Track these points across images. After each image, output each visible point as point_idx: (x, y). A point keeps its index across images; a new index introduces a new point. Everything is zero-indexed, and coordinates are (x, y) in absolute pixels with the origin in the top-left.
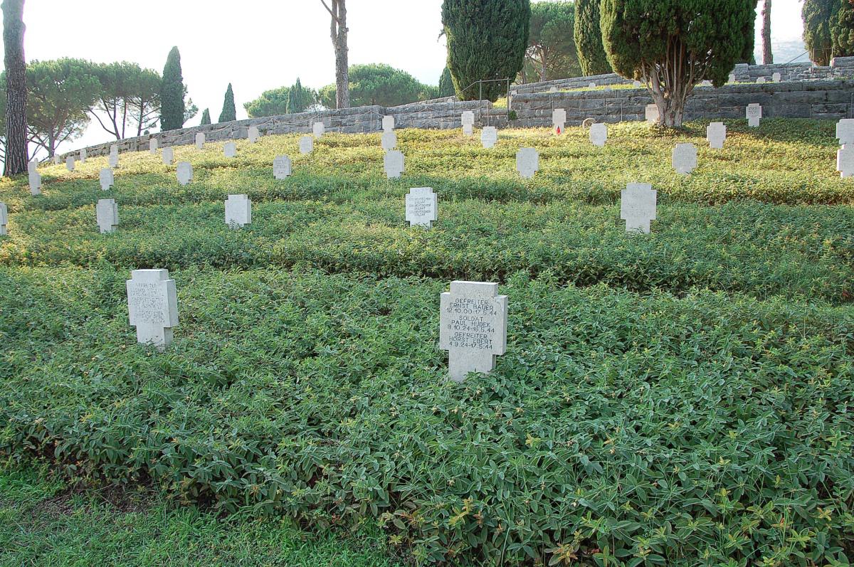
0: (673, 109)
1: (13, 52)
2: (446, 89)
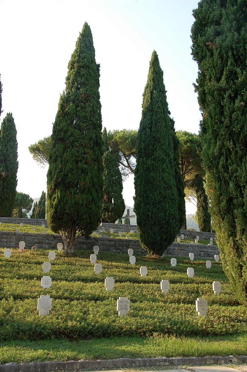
0: (71, 246)
1: (207, 279)
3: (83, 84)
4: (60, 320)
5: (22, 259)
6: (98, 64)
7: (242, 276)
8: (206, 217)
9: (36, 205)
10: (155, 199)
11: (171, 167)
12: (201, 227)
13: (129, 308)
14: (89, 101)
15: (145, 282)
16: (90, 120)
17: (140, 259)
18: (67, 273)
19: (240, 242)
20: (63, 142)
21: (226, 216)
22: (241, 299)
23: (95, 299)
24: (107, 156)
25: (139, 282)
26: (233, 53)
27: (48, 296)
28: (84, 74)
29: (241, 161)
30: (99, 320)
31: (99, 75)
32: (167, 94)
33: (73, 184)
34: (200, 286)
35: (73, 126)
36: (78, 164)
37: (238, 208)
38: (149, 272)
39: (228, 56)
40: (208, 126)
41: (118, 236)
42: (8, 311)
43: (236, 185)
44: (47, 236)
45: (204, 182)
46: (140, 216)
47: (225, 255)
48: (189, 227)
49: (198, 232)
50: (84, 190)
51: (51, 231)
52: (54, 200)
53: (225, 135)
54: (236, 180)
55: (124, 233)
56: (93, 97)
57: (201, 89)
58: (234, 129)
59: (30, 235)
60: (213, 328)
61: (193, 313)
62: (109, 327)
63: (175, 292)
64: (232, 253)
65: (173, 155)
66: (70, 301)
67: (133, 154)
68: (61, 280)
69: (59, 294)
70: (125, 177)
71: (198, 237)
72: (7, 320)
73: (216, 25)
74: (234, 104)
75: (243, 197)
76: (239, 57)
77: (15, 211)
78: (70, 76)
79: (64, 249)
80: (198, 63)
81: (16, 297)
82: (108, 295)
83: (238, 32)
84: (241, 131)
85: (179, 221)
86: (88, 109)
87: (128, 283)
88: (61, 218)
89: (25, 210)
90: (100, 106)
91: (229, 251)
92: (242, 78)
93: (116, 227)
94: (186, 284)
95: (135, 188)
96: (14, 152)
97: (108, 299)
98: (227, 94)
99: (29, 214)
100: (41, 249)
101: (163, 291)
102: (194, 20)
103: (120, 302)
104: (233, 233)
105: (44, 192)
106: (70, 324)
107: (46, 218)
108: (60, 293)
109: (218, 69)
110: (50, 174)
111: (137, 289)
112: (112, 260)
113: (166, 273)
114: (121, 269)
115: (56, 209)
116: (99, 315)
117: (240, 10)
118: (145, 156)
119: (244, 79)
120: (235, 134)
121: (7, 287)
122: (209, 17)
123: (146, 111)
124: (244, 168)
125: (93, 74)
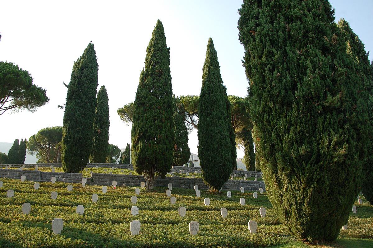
2: (12, 155)
3: (158, 63)
4: (147, 239)
5: (115, 194)
6: (169, 47)
7: (283, 203)
8: (252, 160)
9: (122, 154)
10: (214, 147)
11: (225, 123)
12: (248, 168)
13: (198, 229)
14: (162, 75)
15: (208, 210)
16: (164, 89)
17: (203, 193)
18: (149, 204)
19: (281, 177)
20: (143, 106)
21: (270, 158)
22: (281, 219)
23: (172, 223)
24: (176, 116)
25: (204, 210)
26: (269, 39)
27: (137, 221)
28: (159, 55)
29: (280, 117)
30: (177, 238)
31: (169, 56)
32: (220, 68)
33: (152, 137)
34: (250, 211)
35: (151, 93)
36: (155, 122)
37: (279, 152)
38: (211, 203)
39: (266, 41)
40: (254, 91)
41: (186, 176)
42: (109, 231)
43: (276, 134)
44: (133, 176)
45: (252, 133)
46: (202, 160)
47: (269, 187)
48: (238, 168)
49: (246, 172)
50: (160, 142)
51: (135, 172)
52: (138, 150)
53: (267, 98)
54: (277, 131)
55: (190, 173)
56: (165, 72)
57: (247, 64)
58: (273, 93)
59: (120, 176)
60: (262, 241)
61: (246, 231)
62: (184, 243)
63: (232, 217)
64: (275, 185)
65: (227, 114)
66: (153, 225)
67: (196, 113)
68: (145, 209)
69: (144, 220)
70: (189, 131)
71: (246, 175)
72: (109, 238)
73: (256, 19)
74: (273, 75)
75: (282, 144)
76: (274, 42)
77: (108, 158)
78: (148, 57)
79: (145, 186)
80: (244, 45)
81: (114, 222)
82: (181, 220)
83: (272, 24)
84: (279, 94)
85: (232, 163)
86: (162, 81)
87: (196, 211)
88: (143, 163)
89: (115, 157)
90: (171, 78)
91: (273, 184)
92: (278, 56)
93: (184, 169)
94: (239, 211)
95: (199, 139)
96: (106, 114)
97: (182, 222)
98: (267, 68)
99: (118, 161)
100: (129, 187)
101: (222, 216)
102: (239, 16)
103: (192, 225)
104: (275, 170)
105: (129, 144)
106: (155, 241)
107: (130, 164)
108: (146, 219)
109: (259, 50)
110: (134, 131)
111: (203, 215)
112: (182, 194)
113: (224, 203)
114: (190, 201)
115: (139, 156)
116: (176, 235)
117: (272, 10)
118: (205, 115)
119: (278, 57)
120: (274, 97)
121: (106, 215)
122: (250, 14)
123: (205, 81)
124: (282, 122)
125: (165, 55)
